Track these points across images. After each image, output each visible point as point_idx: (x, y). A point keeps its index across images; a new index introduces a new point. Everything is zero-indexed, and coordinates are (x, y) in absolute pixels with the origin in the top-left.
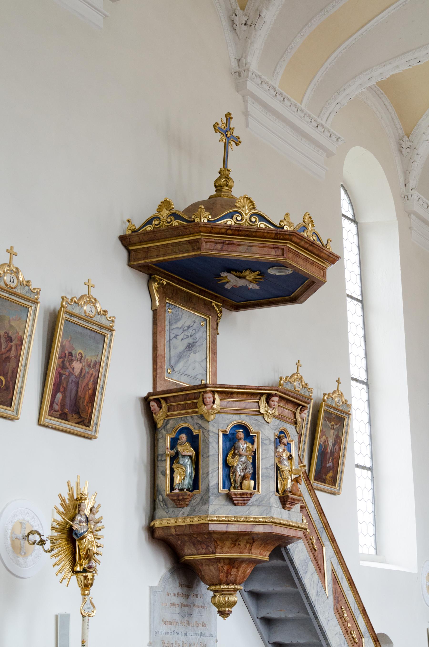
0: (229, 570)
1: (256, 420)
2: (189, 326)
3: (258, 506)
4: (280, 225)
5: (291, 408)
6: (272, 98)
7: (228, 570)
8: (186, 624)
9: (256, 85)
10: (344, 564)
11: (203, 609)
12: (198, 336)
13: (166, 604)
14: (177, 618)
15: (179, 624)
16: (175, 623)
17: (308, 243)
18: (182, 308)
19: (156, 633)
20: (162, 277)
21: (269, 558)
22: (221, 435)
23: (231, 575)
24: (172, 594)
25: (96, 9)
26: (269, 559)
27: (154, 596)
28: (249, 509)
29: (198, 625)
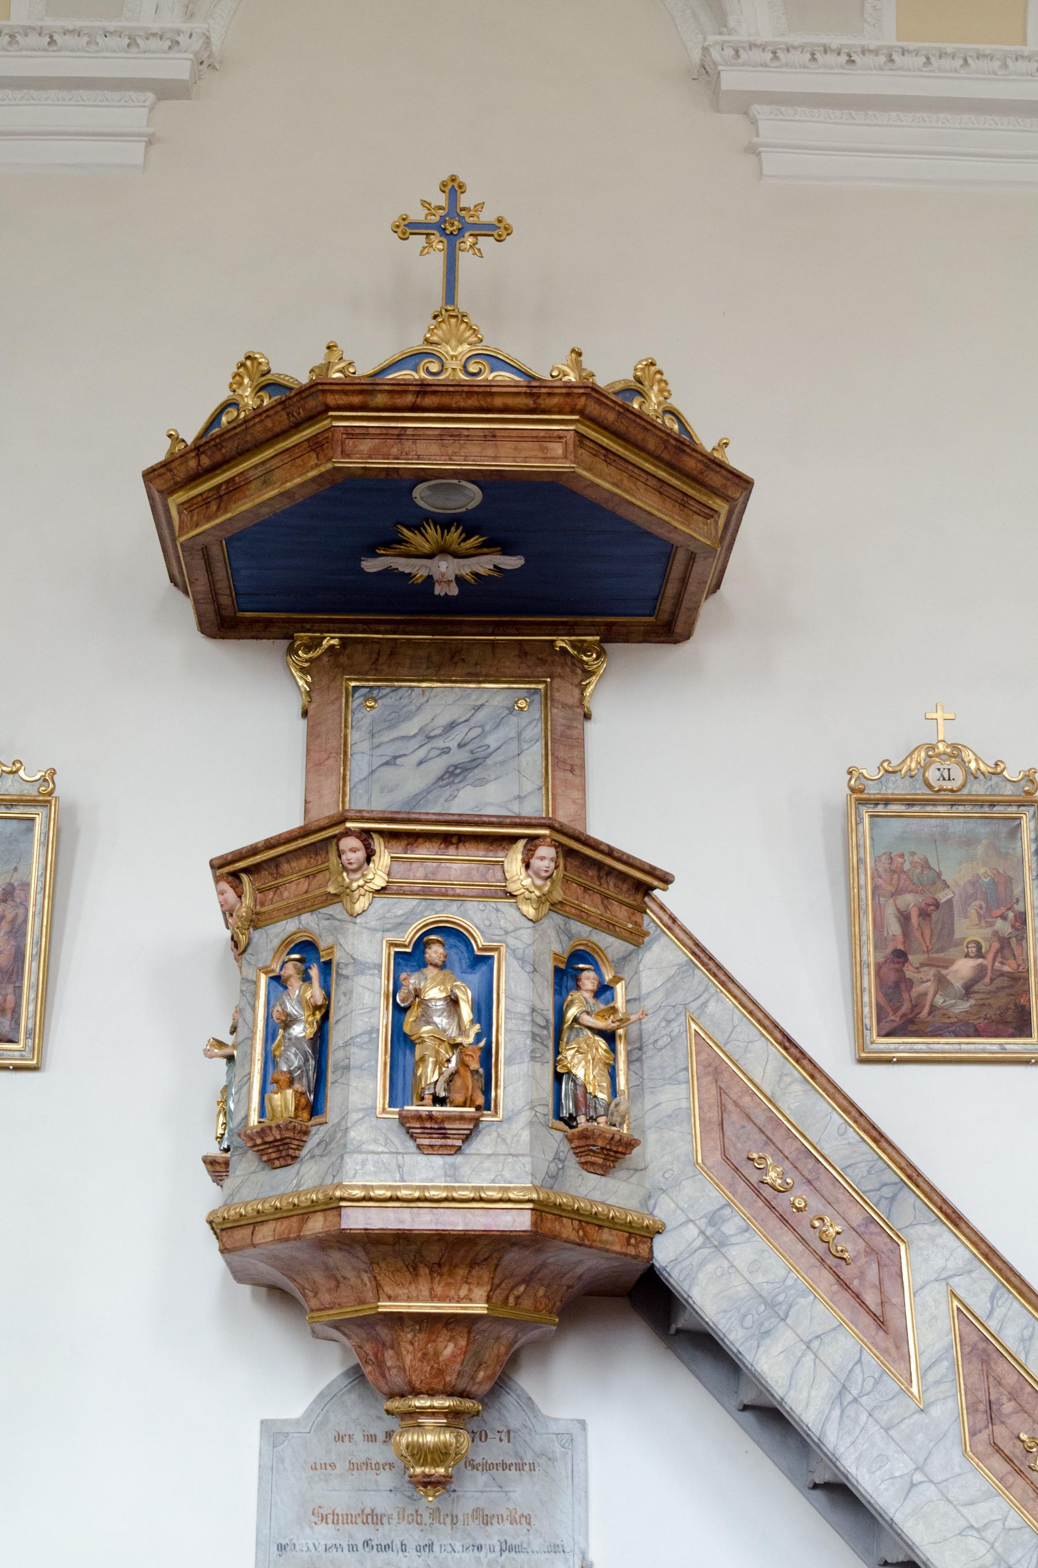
0: (379, 1355)
1: (331, 917)
2: (453, 722)
3: (322, 1156)
4: (552, 376)
5: (482, 853)
6: (841, 74)
7: (376, 1356)
8: (426, 1519)
9: (761, 69)
10: (1024, 1289)
11: (513, 1473)
12: (492, 741)
13: (333, 1466)
14: (383, 1502)
15: (394, 1521)
16: (374, 1518)
17: (406, 392)
18: (424, 685)
19: (281, 1548)
20: (322, 632)
21: (486, 1305)
22: (263, 979)
23: (389, 1369)
24: (358, 1437)
25: (71, 134)
26: (488, 1309)
27: (274, 1446)
28: (298, 1173)
29: (486, 1519)
